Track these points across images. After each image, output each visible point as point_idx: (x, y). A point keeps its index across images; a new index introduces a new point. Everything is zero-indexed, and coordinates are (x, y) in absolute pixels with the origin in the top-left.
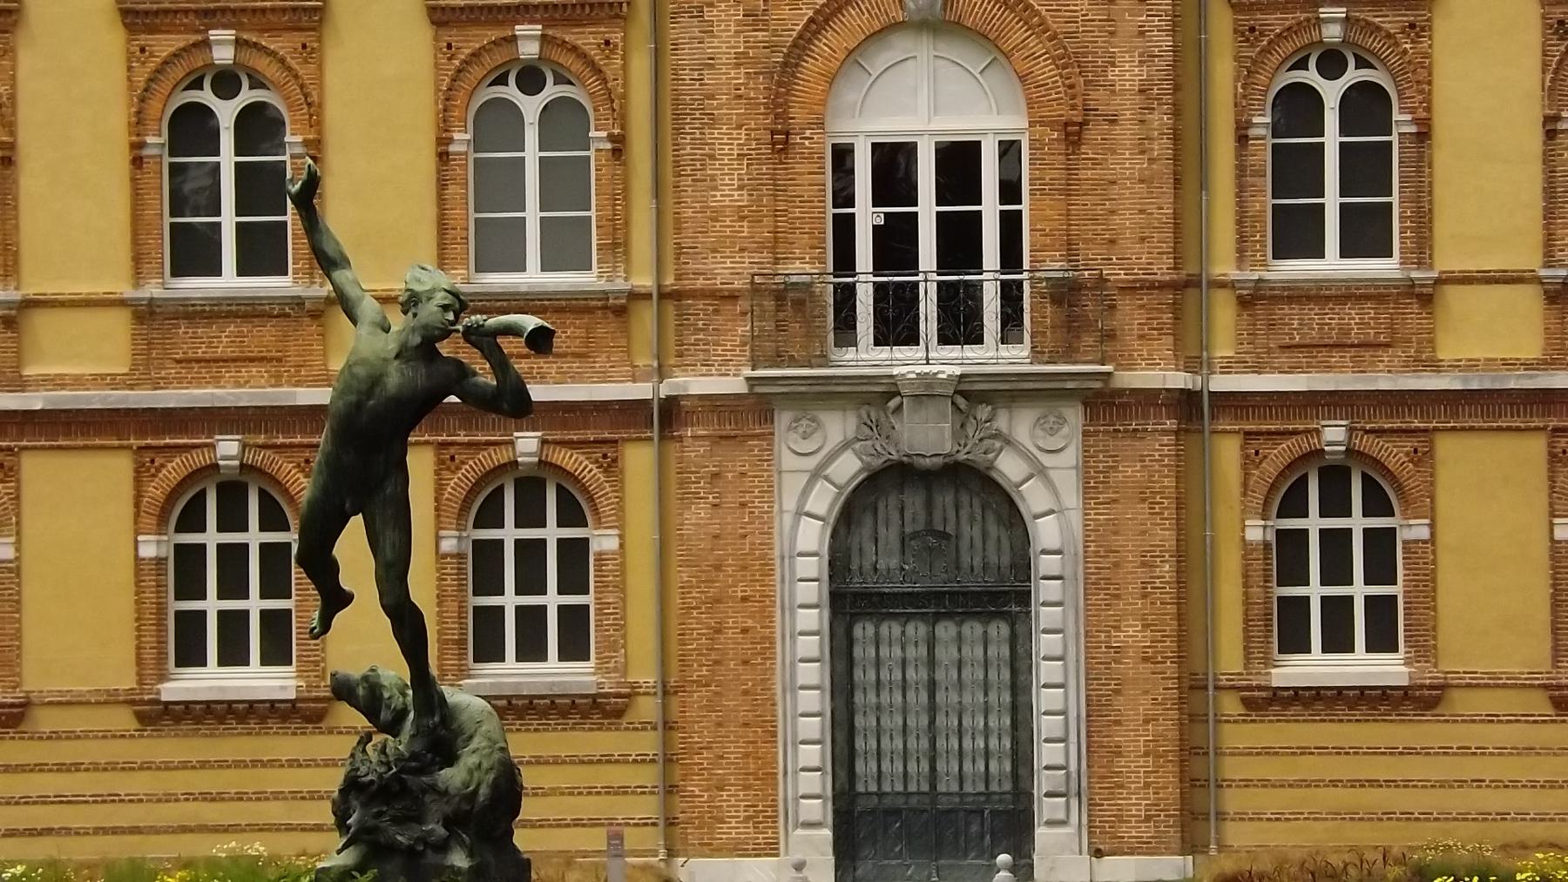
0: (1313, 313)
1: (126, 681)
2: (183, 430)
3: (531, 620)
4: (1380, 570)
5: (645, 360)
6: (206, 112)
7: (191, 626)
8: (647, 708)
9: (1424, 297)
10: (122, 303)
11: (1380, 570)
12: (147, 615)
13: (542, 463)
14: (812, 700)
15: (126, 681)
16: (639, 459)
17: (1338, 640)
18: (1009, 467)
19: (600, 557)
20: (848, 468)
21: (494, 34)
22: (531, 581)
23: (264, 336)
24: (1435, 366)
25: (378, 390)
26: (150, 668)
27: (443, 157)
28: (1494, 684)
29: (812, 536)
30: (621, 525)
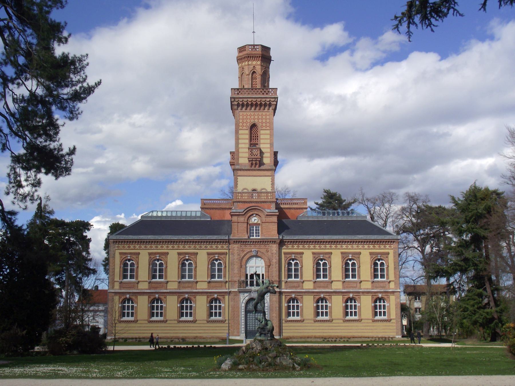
0: (291, 284)
5: (227, 287)
6: (349, 263)
7: (124, 313)
8: (227, 322)
10: (147, 281)
13: (353, 297)
14: (243, 321)
16: (227, 297)
20: (247, 298)
21: (213, 256)
23: (190, 285)
27: (208, 268)
28: (338, 319)
29: (243, 305)
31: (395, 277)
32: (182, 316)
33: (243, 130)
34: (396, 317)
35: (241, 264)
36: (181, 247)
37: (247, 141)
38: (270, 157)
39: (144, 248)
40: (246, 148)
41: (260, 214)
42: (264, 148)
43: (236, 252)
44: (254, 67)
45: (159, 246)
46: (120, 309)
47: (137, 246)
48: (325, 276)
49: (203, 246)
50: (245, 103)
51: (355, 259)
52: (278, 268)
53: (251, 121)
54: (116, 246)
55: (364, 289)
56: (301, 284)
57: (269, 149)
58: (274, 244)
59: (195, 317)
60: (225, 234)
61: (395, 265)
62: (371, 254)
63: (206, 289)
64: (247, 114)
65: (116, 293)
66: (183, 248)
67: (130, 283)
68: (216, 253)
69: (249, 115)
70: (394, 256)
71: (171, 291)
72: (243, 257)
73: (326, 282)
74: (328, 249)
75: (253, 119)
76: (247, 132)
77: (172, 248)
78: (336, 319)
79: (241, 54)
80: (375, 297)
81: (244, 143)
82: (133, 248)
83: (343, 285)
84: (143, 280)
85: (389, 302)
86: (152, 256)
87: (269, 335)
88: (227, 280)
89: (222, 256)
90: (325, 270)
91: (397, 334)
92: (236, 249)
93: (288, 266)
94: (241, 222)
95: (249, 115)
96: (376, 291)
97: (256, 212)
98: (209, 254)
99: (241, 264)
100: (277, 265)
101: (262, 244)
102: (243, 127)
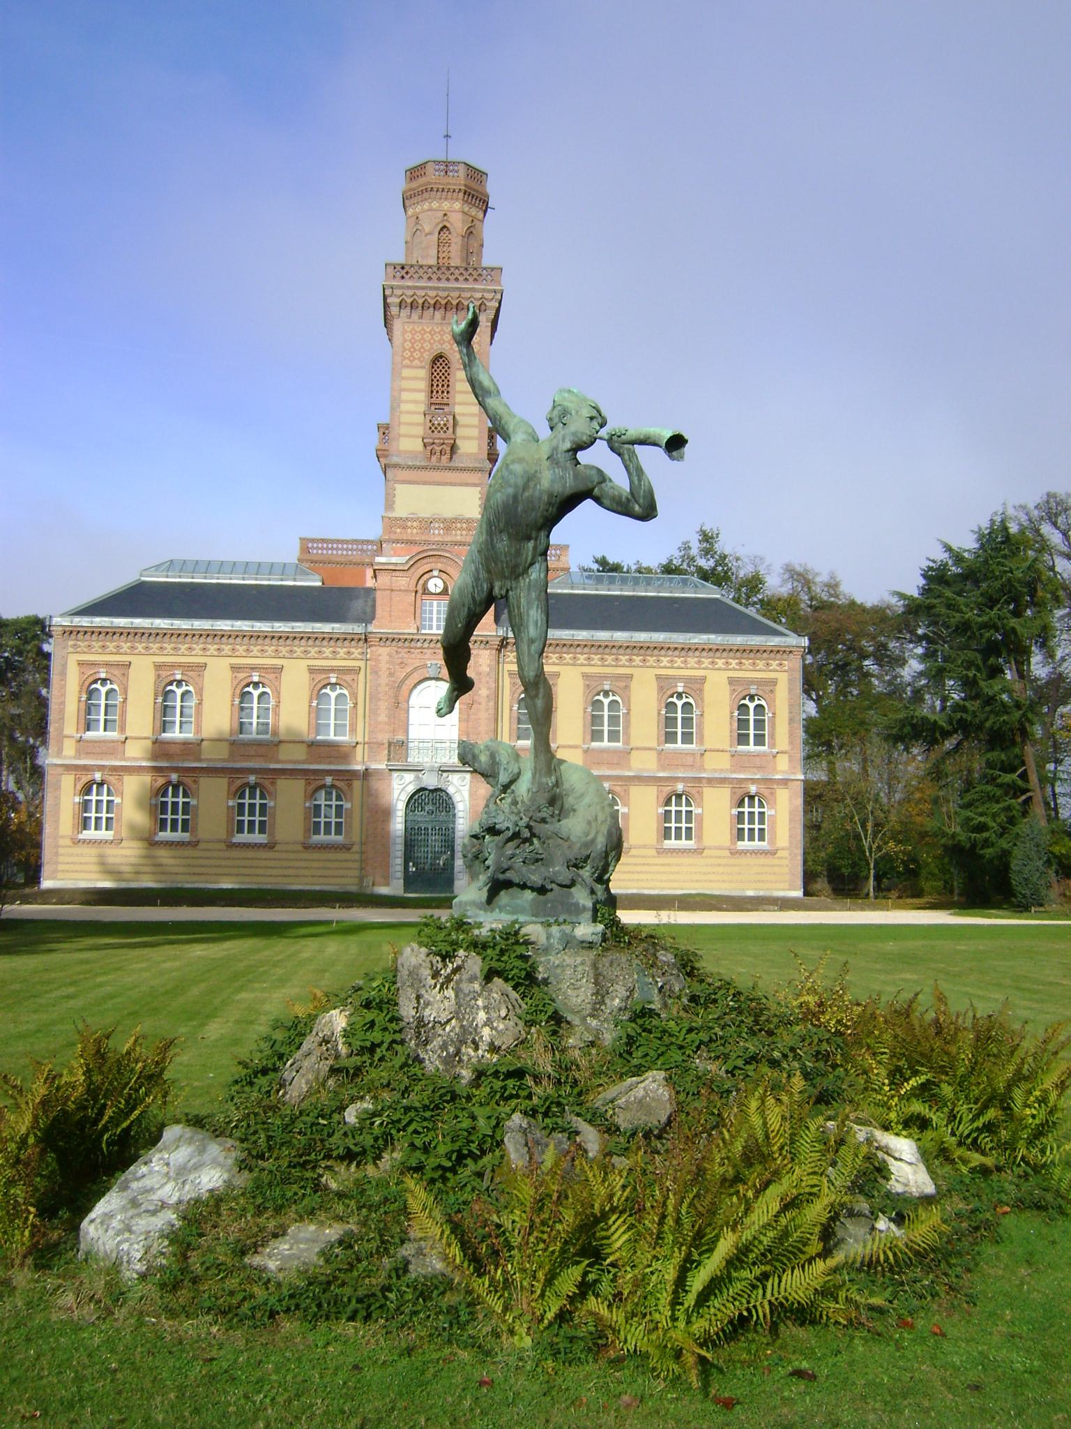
1: (301, 839)
2: (242, 773)
3: (678, 829)
4: (689, 820)
6: (675, 704)
7: (241, 823)
8: (356, 848)
9: (628, 753)
11: (689, 820)
12: (230, 820)
15: (301, 839)
17: (678, 837)
18: (451, 790)
19: (346, 809)
20: (411, 789)
22: (678, 820)
24: (630, 770)
25: (532, 484)
26: (230, 833)
28: (644, 847)
30: (352, 802)
31: (791, 743)
32: (85, 828)
33: (413, 367)
34: (791, 843)
35: (396, 697)
36: (241, 650)
37: (422, 396)
38: (479, 438)
39: (143, 651)
40: (418, 413)
41: (449, 570)
42: (463, 415)
43: (384, 666)
44: (445, 215)
45: (183, 647)
46: (77, 810)
47: (126, 646)
48: (614, 736)
49: (299, 651)
50: (420, 301)
51: (692, 693)
52: (492, 711)
53: (434, 346)
54: (71, 643)
55: (715, 771)
56: (120, 746)
57: (477, 419)
58: (485, 649)
59: (272, 834)
60: (358, 620)
61: (791, 713)
62: (732, 681)
63: (303, 762)
64: (423, 329)
65: (68, 768)
66: (244, 654)
67: (104, 741)
68: (332, 670)
69: (430, 332)
70: (790, 690)
71: (211, 765)
72: (403, 681)
73: (616, 751)
74: (623, 666)
75: (439, 342)
76: (423, 373)
77: (216, 653)
78: (710, 848)
79: (414, 185)
80: (740, 793)
81: (415, 402)
82: (114, 650)
83: (659, 760)
84: (714, 747)
85: (773, 805)
86: (164, 674)
87: (582, 897)
88: (360, 739)
89: (348, 678)
90: (614, 720)
91: (791, 888)
92: (384, 658)
93: (241, 702)
94: (400, 590)
95: (430, 332)
96: (742, 776)
97: (440, 566)
98: (312, 670)
99: (396, 697)
100: (492, 704)
101: (428, 648)
102: (412, 361)
